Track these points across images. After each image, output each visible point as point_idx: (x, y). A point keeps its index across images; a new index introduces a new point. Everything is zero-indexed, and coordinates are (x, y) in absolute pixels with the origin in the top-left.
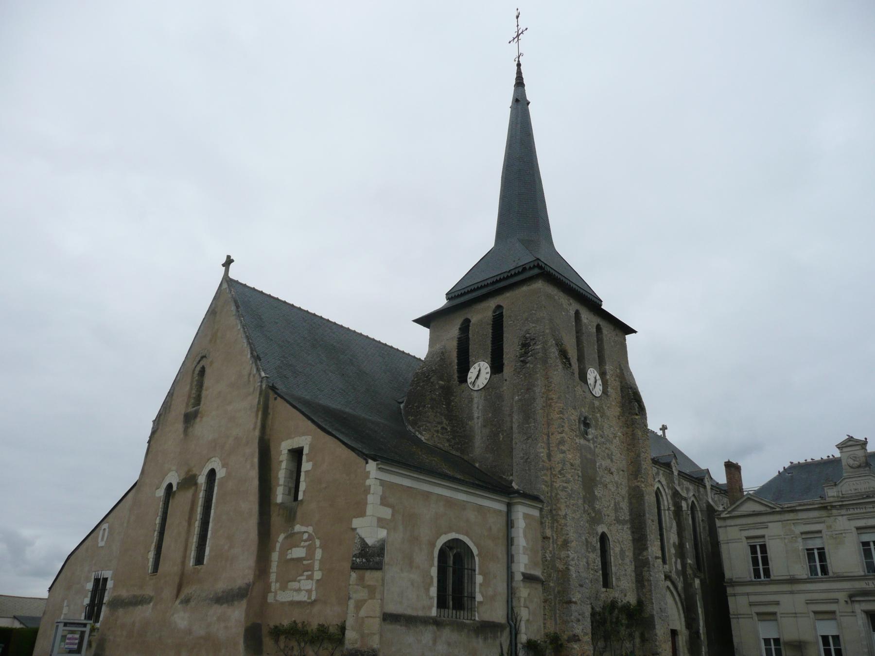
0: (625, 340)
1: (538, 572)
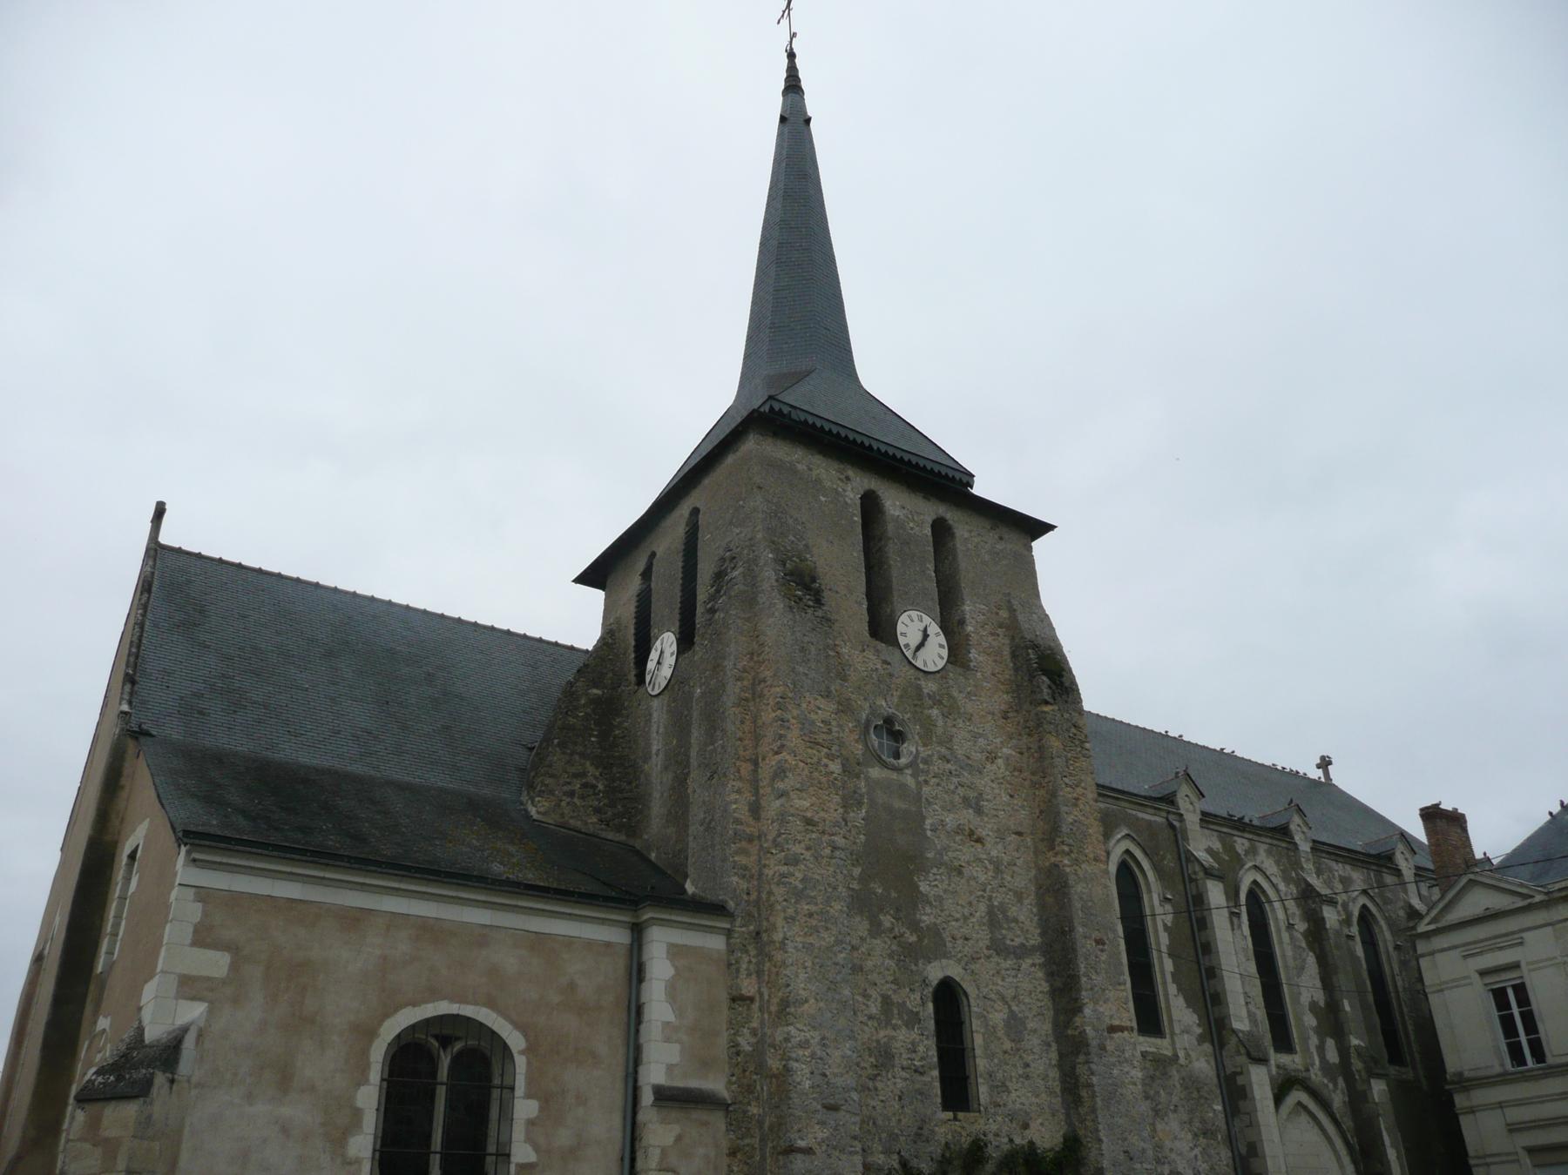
0: (1030, 549)
1: (716, 1084)
